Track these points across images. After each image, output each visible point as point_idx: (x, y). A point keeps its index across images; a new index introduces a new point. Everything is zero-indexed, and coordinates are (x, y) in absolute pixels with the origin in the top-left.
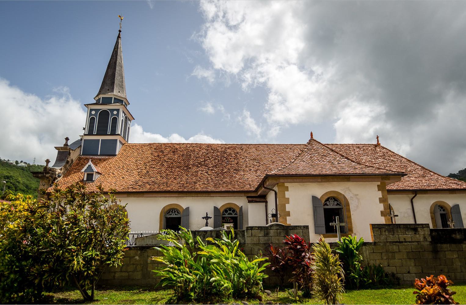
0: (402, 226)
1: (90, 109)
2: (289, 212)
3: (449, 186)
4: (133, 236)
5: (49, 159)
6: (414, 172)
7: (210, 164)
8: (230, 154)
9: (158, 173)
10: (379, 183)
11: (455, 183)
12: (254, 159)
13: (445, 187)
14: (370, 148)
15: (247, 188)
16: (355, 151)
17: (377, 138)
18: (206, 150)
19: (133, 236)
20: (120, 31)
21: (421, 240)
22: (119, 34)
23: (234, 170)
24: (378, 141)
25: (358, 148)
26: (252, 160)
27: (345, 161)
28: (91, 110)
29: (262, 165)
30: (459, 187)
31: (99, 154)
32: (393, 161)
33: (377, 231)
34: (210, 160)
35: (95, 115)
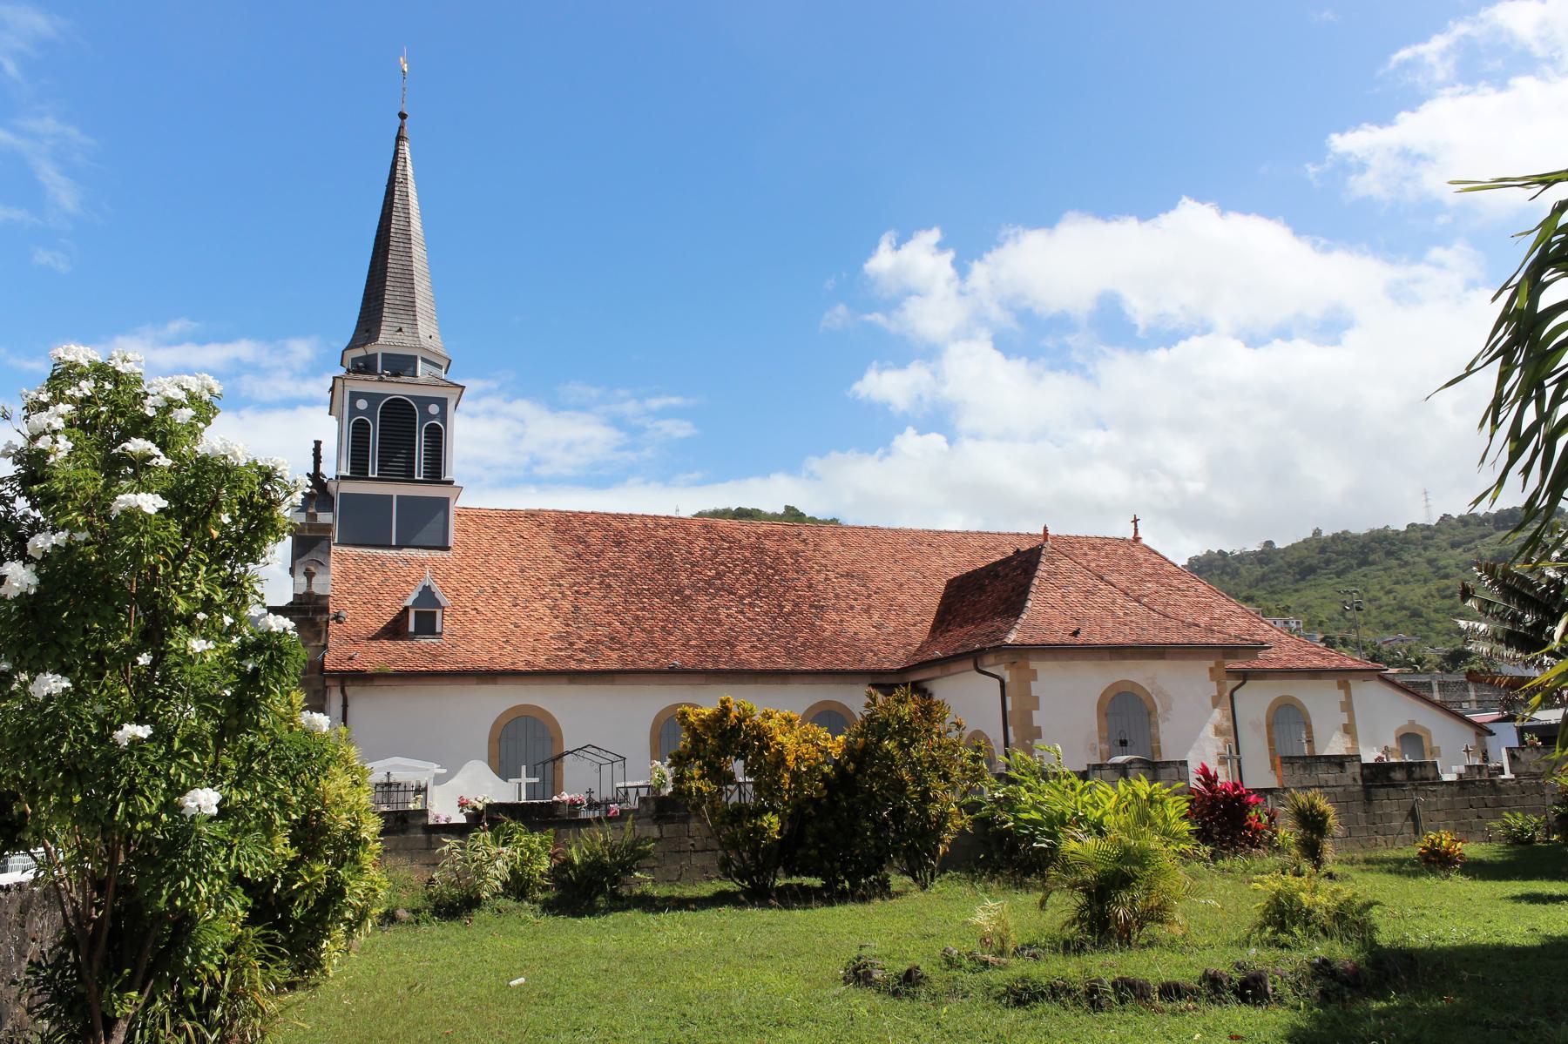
0: (1323, 760)
1: (351, 392)
2: (1039, 729)
3: (1307, 661)
4: (637, 793)
5: (1338, 706)
6: (1228, 622)
7: (738, 585)
8: (778, 558)
9: (608, 612)
10: (1211, 663)
11: (1315, 653)
12: (848, 575)
13: (1299, 664)
14: (1120, 552)
15: (871, 662)
16: (1089, 558)
17: (1135, 521)
18: (705, 539)
19: (637, 793)
20: (403, 116)
21: (261, 973)
22: (401, 127)
23: (811, 606)
24: (1136, 530)
25: (1094, 547)
26: (842, 576)
27: (1135, 607)
28: (355, 396)
29: (876, 593)
30: (1325, 664)
31: (394, 543)
32: (1179, 589)
33: (1288, 768)
34: (731, 572)
35: (370, 411)
